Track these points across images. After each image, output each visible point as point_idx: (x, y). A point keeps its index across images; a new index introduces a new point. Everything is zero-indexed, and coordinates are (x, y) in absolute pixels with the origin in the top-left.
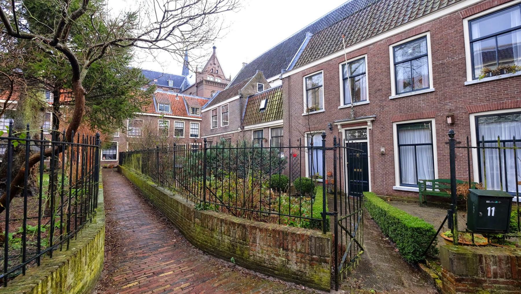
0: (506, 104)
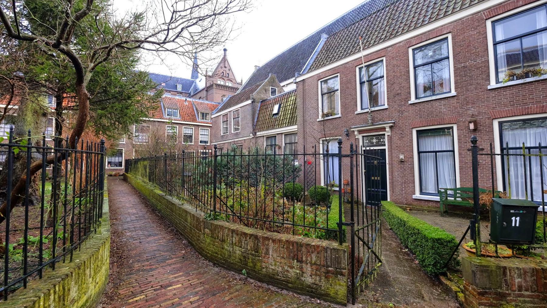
0: (531, 108)
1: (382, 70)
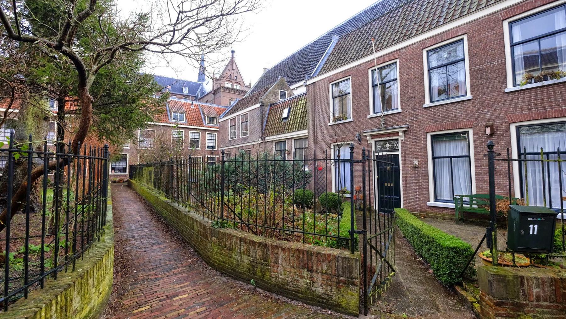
0: (549, 112)
1: (395, 73)
